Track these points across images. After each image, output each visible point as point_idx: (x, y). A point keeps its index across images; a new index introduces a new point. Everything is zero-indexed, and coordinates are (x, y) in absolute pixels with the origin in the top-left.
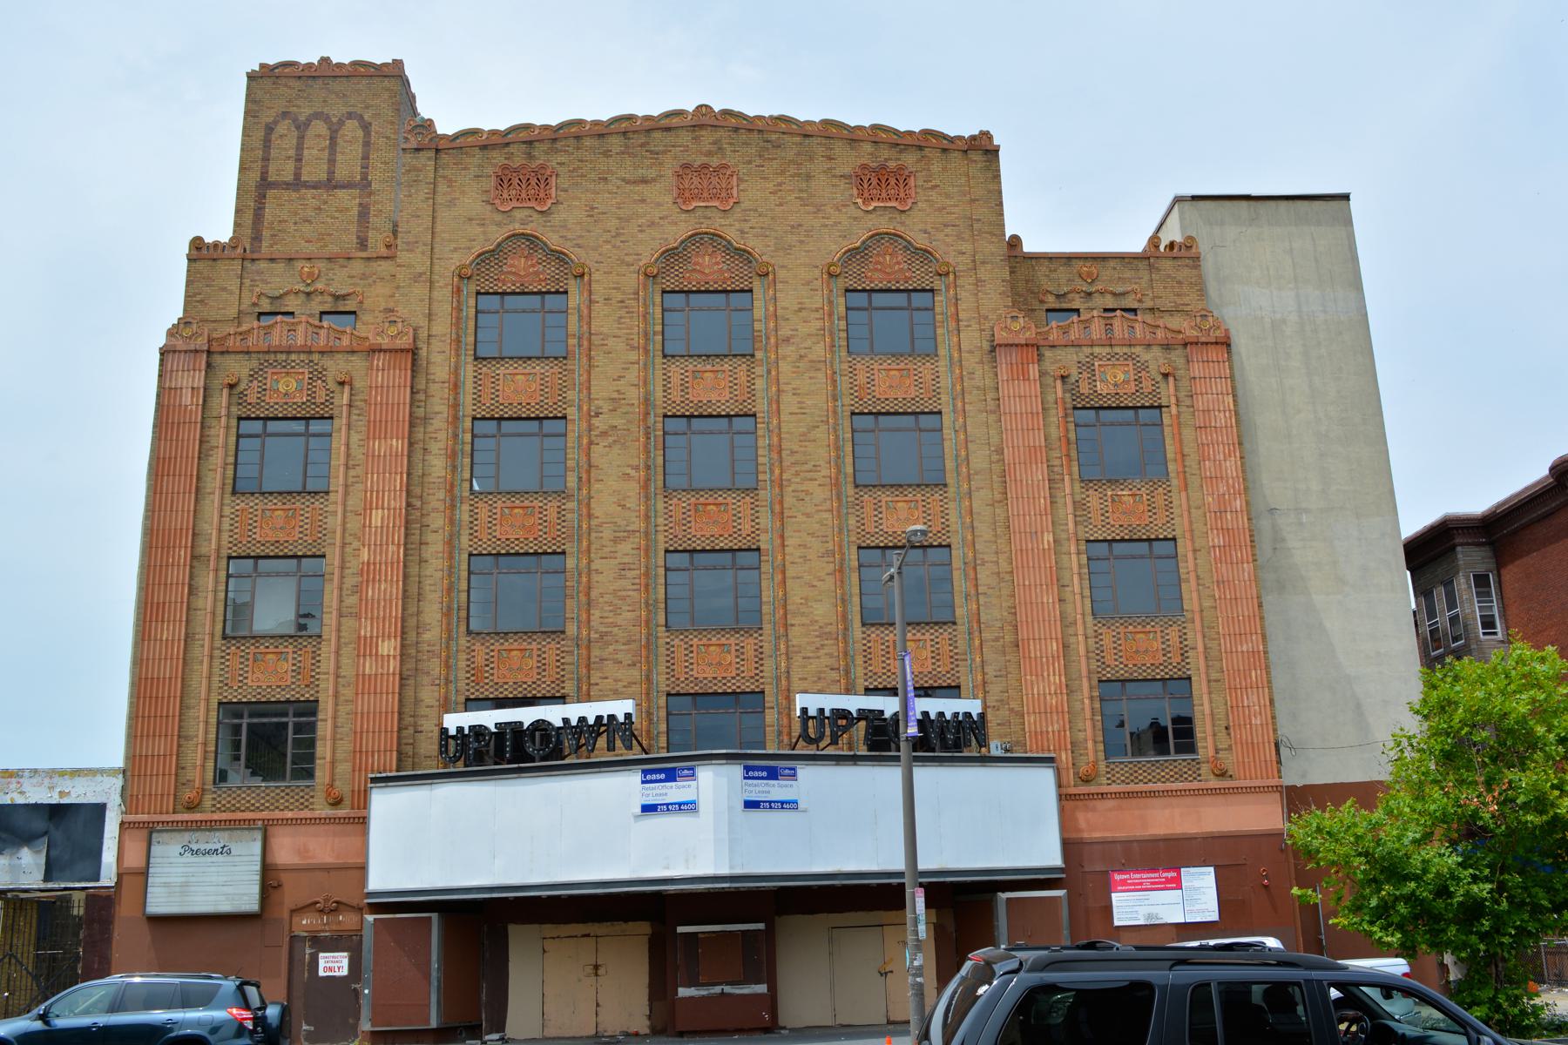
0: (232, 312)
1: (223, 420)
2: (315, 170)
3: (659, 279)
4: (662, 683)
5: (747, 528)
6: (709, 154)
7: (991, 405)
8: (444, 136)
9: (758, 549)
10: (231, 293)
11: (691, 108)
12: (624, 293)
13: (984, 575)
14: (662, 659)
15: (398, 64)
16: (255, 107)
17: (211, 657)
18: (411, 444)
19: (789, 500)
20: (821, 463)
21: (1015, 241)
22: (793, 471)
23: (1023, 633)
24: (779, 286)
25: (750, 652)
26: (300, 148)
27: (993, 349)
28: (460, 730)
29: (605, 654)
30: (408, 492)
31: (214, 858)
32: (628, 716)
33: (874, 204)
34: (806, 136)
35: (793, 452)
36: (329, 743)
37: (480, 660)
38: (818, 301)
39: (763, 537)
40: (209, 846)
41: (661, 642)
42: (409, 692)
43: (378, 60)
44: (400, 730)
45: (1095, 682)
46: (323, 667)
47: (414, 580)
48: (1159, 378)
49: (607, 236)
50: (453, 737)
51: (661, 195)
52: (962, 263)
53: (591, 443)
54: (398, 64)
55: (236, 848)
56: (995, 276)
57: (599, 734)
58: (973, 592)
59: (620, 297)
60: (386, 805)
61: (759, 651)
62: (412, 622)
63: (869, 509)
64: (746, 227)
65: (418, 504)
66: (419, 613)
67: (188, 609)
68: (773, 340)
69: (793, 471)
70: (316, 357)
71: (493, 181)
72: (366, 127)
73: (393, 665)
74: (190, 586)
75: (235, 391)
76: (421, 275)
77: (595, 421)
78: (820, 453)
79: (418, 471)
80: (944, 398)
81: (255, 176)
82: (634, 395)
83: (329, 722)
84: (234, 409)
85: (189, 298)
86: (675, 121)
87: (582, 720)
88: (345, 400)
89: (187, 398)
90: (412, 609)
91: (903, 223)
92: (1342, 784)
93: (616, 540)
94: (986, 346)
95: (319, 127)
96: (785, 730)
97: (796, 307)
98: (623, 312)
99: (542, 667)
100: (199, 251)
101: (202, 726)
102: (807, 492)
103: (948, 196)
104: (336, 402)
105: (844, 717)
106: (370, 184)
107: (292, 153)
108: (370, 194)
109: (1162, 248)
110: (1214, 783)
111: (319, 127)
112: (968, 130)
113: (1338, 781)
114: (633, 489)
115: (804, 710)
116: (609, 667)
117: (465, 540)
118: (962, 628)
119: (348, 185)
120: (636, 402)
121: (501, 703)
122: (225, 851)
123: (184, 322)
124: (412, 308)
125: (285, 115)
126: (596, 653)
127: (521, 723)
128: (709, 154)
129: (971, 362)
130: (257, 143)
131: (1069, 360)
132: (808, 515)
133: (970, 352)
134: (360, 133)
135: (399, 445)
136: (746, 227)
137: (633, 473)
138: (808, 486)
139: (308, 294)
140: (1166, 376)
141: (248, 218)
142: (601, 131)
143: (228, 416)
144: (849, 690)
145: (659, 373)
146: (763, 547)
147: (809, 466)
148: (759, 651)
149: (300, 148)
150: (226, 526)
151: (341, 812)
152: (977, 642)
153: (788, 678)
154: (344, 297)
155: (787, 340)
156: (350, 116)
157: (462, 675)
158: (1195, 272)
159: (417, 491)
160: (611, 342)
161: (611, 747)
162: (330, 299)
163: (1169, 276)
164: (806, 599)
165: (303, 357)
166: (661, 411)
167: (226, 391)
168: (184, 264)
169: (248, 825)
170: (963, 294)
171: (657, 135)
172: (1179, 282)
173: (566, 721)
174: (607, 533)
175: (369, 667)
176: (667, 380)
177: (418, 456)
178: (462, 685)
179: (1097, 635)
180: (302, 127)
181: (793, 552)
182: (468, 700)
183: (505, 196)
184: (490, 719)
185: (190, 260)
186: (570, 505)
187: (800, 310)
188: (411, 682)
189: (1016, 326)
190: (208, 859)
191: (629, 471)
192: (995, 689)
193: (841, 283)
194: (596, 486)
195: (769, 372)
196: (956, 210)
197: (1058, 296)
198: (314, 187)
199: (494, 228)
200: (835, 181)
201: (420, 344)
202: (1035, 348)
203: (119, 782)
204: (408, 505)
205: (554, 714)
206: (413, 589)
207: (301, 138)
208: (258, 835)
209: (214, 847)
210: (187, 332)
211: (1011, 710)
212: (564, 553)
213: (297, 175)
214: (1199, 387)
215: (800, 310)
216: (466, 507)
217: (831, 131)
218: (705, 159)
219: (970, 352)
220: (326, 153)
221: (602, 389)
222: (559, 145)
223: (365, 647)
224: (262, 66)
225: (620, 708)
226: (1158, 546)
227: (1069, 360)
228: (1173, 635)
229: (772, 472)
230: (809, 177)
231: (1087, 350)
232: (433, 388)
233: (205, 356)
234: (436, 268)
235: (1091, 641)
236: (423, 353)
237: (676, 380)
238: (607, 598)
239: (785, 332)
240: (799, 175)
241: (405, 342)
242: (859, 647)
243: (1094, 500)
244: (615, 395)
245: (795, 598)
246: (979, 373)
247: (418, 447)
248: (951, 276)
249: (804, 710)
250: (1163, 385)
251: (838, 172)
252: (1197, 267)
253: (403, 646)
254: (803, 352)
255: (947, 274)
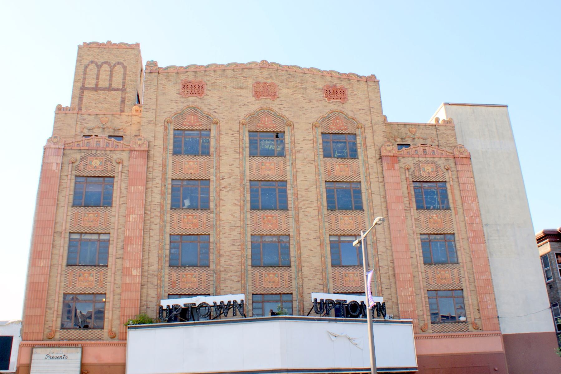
0: (73, 134)
1: (69, 176)
2: (103, 83)
3: (247, 126)
4: (250, 290)
5: (284, 226)
6: (267, 78)
7: (381, 179)
8: (161, 68)
9: (289, 235)
10: (72, 127)
11: (259, 61)
12: (233, 131)
13: (381, 248)
14: (250, 279)
15: (138, 45)
16: (80, 59)
17: (61, 274)
18: (146, 189)
19: (301, 215)
20: (314, 201)
21: (385, 118)
22: (303, 203)
23: (397, 271)
24: (295, 130)
25: (286, 278)
26: (98, 75)
27: (381, 158)
28: (168, 306)
29: (227, 277)
30: (145, 208)
31: (60, 360)
32: (242, 301)
33: (332, 100)
34: (305, 73)
35: (302, 196)
36: (111, 312)
37: (174, 278)
38: (311, 137)
39: (291, 230)
40: (58, 355)
41: (250, 272)
42: (145, 291)
43: (130, 43)
44: (140, 306)
45: (426, 291)
46: (109, 279)
47: (147, 244)
48: (445, 171)
49: (227, 109)
50: (165, 310)
51: (248, 94)
52: (367, 124)
53: (221, 190)
54: (138, 45)
55: (69, 356)
56: (379, 129)
57: (229, 309)
58: (376, 254)
59: (232, 133)
60: (136, 338)
61: (290, 277)
62: (146, 262)
63: (333, 220)
64: (282, 107)
65: (149, 213)
66: (149, 258)
67: (52, 254)
68: (294, 151)
69: (303, 203)
70: (108, 152)
71: (181, 86)
72: (125, 68)
73: (138, 280)
74: (53, 244)
75: (74, 165)
76: (151, 121)
77: (222, 181)
78: (313, 196)
79: (149, 200)
80: (362, 176)
81: (79, 85)
82: (237, 171)
83: (111, 303)
84: (74, 172)
85: (55, 129)
86: (253, 66)
87: (222, 302)
88: (120, 170)
89: (54, 167)
90: (146, 256)
91: (343, 108)
92: (519, 334)
93: (231, 230)
94: (378, 157)
95: (106, 67)
96: (302, 310)
97: (303, 139)
98: (233, 139)
99: (200, 281)
100: (59, 109)
101: (56, 303)
102: (308, 212)
103: (360, 98)
104: (116, 170)
105: (331, 303)
106: (125, 90)
107: (95, 76)
108: (126, 93)
109: (440, 122)
110: (475, 332)
111: (106, 67)
112: (367, 74)
113: (517, 333)
114: (237, 209)
115: (316, 300)
116: (228, 283)
117: (168, 229)
118: (293, 268)
119: (117, 90)
120: (239, 174)
121: (180, 296)
122: (64, 357)
123: (54, 136)
124: (147, 133)
125: (92, 62)
126: (223, 276)
127: (195, 304)
128: (267, 78)
129: (372, 162)
130: (81, 71)
131: (409, 162)
132: (309, 222)
133: (371, 158)
134: (122, 70)
135: (141, 188)
136: (282, 107)
137: (238, 203)
138: (309, 210)
139: (104, 128)
140: (448, 170)
141: (77, 101)
142: (224, 69)
143: (71, 175)
144: (328, 292)
145: (248, 163)
146: (291, 234)
147: (309, 202)
148: (290, 277)
149: (98, 75)
150: (69, 220)
151: (116, 341)
152: (378, 274)
153: (302, 288)
154: (118, 130)
155: (299, 152)
156: (119, 63)
157: (167, 284)
158: (453, 132)
159: (148, 208)
160: (228, 150)
161: (235, 315)
162: (112, 130)
163: (444, 133)
164: (309, 256)
165: (103, 152)
166: (249, 178)
167: (71, 165)
168: (53, 115)
169: (76, 346)
170: (367, 136)
171: (246, 70)
172: (448, 135)
173: (215, 303)
174: (227, 227)
175: (128, 280)
176: (251, 166)
177: (149, 193)
178: (167, 289)
179: (426, 272)
180: (99, 67)
181: (303, 236)
182: (169, 295)
183: (186, 91)
184: (181, 302)
185: (56, 113)
186: (212, 215)
187: (304, 140)
188: (145, 287)
189: (389, 148)
190: (57, 360)
191: (236, 202)
192: (386, 293)
193: (320, 130)
194: (222, 208)
195: (292, 164)
196: (364, 104)
197: (402, 139)
198: (103, 90)
199: (181, 104)
200: (316, 91)
201: (151, 149)
202: (395, 159)
203: (20, 327)
204: (145, 213)
205: (210, 300)
206: (147, 248)
207: (99, 71)
208: (79, 350)
209: (60, 355)
210: (55, 140)
211: (393, 302)
212: (209, 235)
213: (97, 85)
214: (460, 174)
215: (304, 140)
216: (169, 215)
217: (312, 72)
218: (265, 81)
219: (371, 158)
220: (109, 77)
221: (225, 169)
222: (207, 73)
223: (126, 272)
224: (84, 43)
225: (239, 298)
226: (448, 238)
227: (409, 162)
228: (455, 272)
229: (294, 203)
230: (306, 89)
231: (417, 159)
232: (156, 166)
233: (62, 150)
234: (157, 119)
235: (424, 274)
236: (152, 152)
237: (254, 166)
238: (227, 254)
239: (298, 148)
240: (302, 88)
241: (145, 148)
242: (331, 275)
243: (422, 218)
244: (230, 171)
245: (304, 256)
246: (375, 168)
247: (149, 190)
248: (363, 129)
249: (316, 300)
250: (446, 174)
251: (317, 87)
252: (454, 130)
253: (142, 272)
254: (305, 156)
255: (362, 128)
